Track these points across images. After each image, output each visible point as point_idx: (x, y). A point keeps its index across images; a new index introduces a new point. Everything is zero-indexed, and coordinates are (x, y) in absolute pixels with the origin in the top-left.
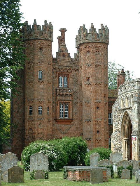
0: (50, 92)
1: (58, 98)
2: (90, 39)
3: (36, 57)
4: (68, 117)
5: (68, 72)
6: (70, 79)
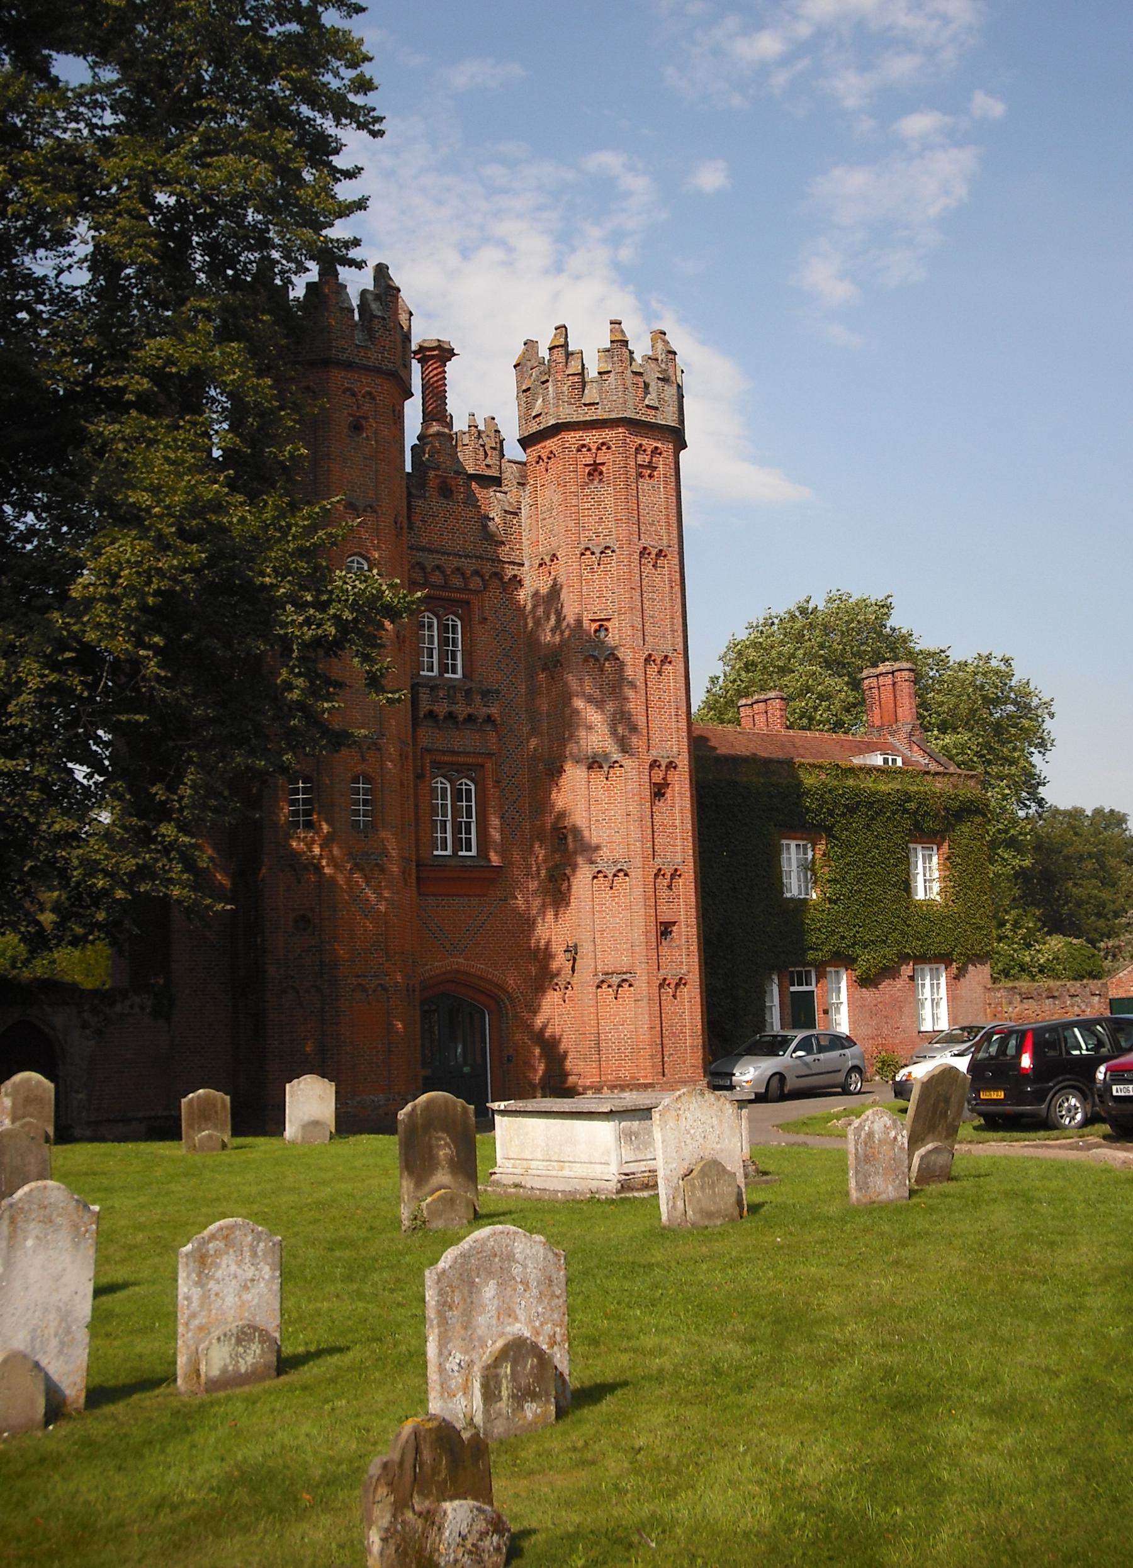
1: (428, 736)
4: (473, 853)
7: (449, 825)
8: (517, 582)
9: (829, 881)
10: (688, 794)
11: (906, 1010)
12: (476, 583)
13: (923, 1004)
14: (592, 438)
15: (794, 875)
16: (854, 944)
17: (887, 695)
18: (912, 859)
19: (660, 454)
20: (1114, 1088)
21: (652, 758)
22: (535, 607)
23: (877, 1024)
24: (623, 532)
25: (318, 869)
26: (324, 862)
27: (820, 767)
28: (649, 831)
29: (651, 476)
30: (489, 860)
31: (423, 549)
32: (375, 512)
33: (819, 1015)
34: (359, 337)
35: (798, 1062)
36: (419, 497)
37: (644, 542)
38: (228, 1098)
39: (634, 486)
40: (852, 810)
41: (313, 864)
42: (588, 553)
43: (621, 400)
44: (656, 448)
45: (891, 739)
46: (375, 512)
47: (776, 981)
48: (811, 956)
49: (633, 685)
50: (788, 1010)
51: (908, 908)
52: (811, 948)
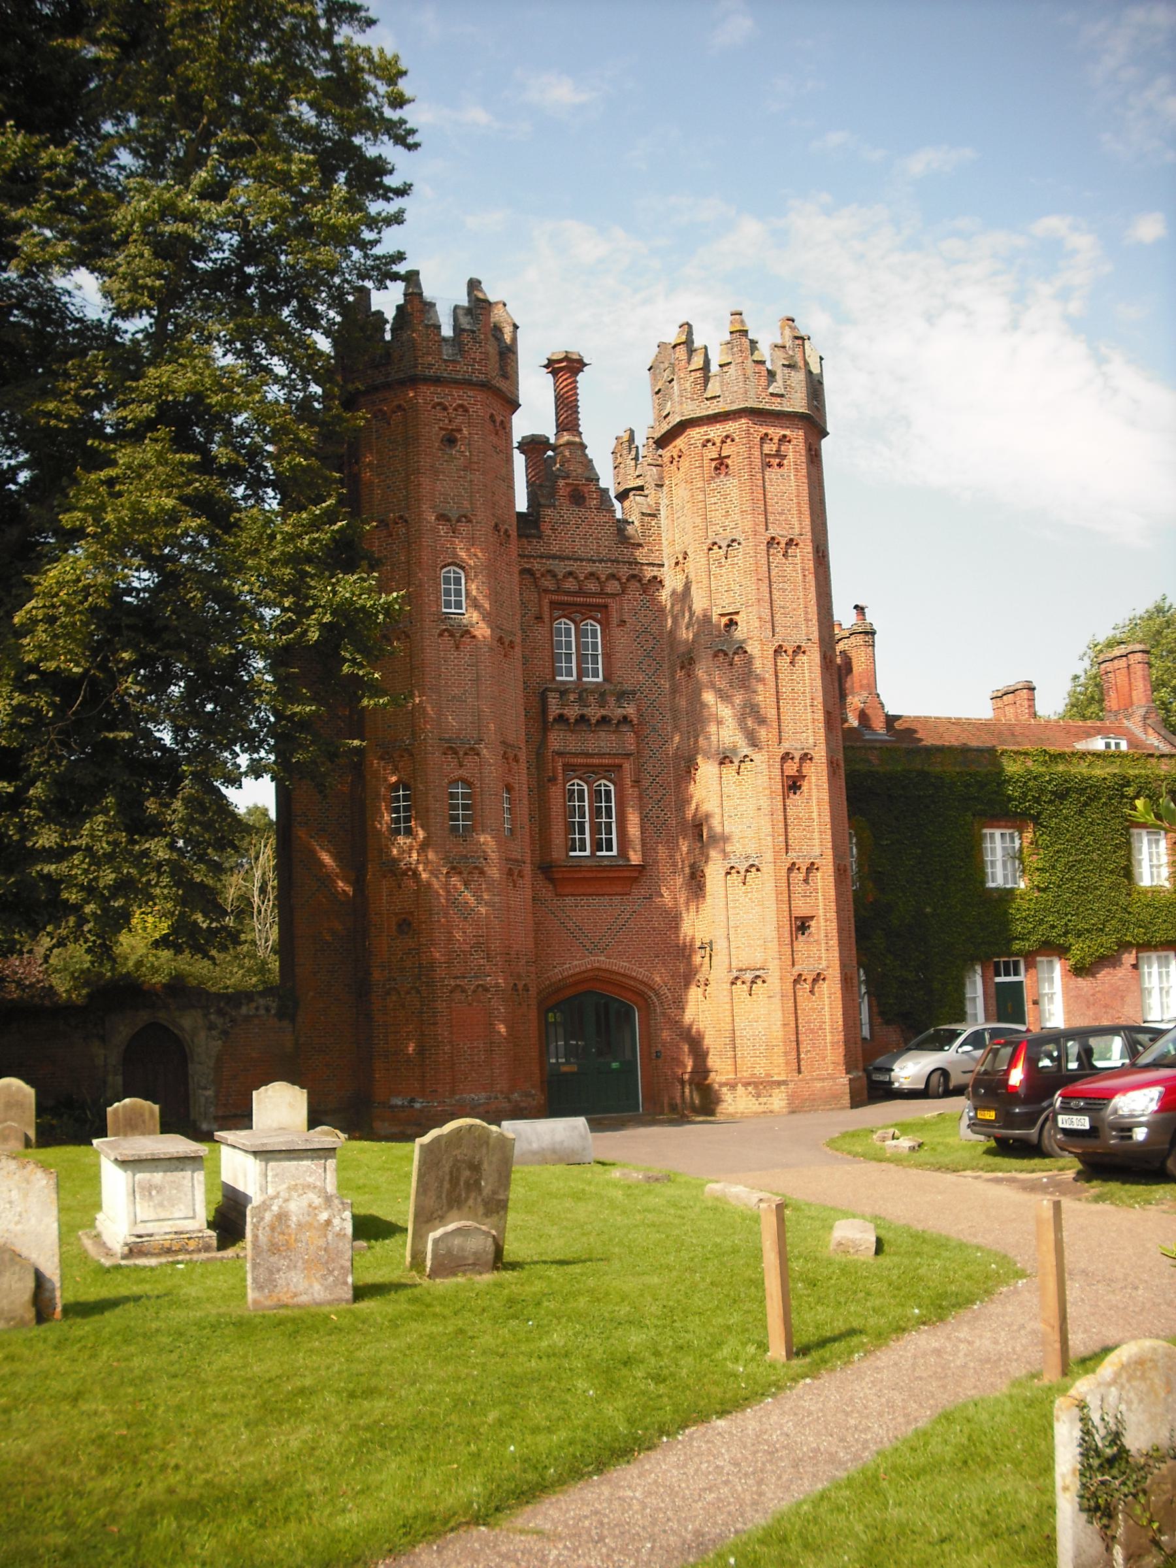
0: (515, 696)
1: (557, 740)
2: (730, 390)
3: (425, 481)
4: (614, 853)
5: (602, 593)
6: (617, 632)
7: (587, 826)
8: (657, 582)
9: (1038, 869)
10: (826, 786)
11: (1128, 999)
12: (613, 587)
13: (1150, 993)
14: (716, 432)
15: (999, 864)
16: (1066, 934)
17: (1121, 679)
18: (1135, 845)
19: (789, 442)
20: (1060, 1117)
21: (783, 751)
22: (673, 605)
23: (1095, 1014)
24: (747, 523)
25: (416, 874)
26: (421, 868)
27: (1026, 754)
28: (782, 825)
29: (780, 465)
30: (628, 860)
31: (554, 557)
32: (470, 521)
33: (1028, 1006)
34: (447, 352)
35: (965, 1057)
36: (549, 507)
37: (772, 532)
38: (156, 1107)
39: (759, 476)
40: (1061, 796)
41: (410, 869)
42: (715, 547)
43: (742, 391)
44: (784, 436)
45: (1126, 723)
46: (470, 521)
47: (979, 971)
48: (1017, 946)
49: (761, 680)
50: (993, 1002)
51: (1129, 895)
52: (1017, 938)
